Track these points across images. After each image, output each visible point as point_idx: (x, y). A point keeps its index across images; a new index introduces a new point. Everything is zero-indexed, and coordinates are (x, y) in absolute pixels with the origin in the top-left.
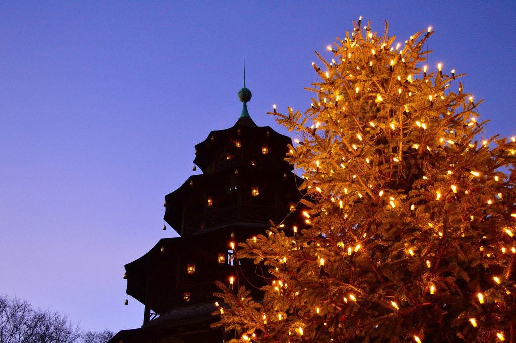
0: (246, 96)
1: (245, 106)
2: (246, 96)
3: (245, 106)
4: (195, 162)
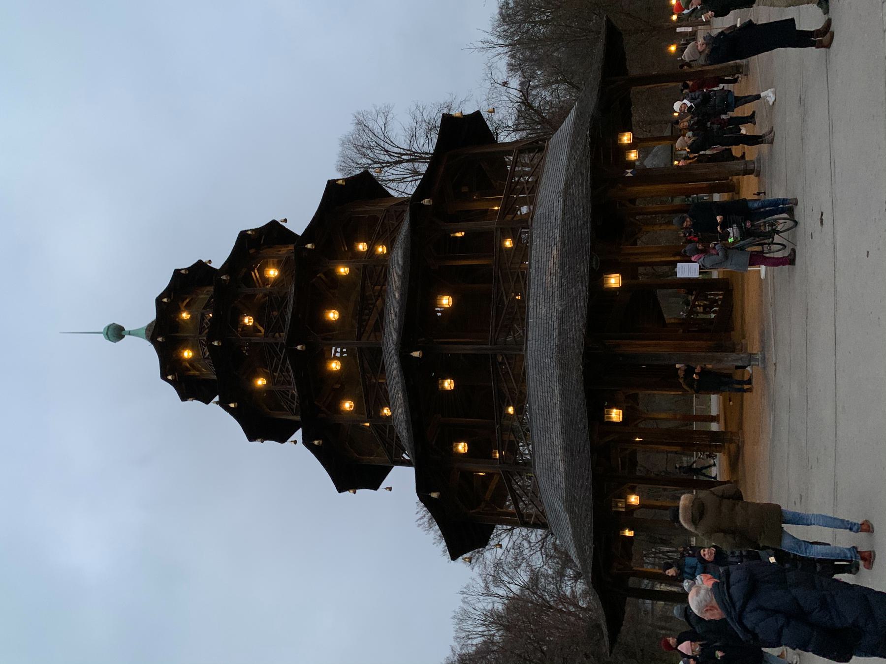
0: (116, 333)
1: (129, 333)
2: (116, 333)
3: (129, 333)
4: (207, 402)
